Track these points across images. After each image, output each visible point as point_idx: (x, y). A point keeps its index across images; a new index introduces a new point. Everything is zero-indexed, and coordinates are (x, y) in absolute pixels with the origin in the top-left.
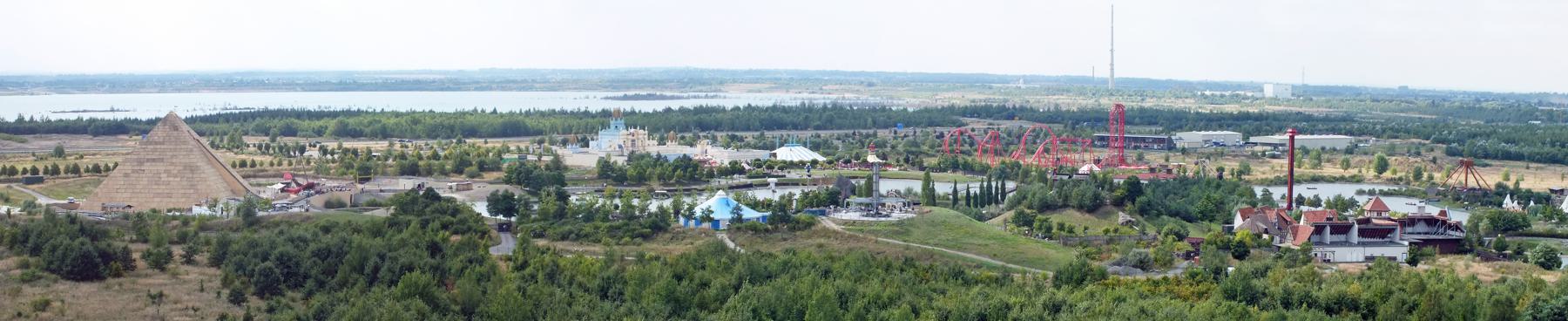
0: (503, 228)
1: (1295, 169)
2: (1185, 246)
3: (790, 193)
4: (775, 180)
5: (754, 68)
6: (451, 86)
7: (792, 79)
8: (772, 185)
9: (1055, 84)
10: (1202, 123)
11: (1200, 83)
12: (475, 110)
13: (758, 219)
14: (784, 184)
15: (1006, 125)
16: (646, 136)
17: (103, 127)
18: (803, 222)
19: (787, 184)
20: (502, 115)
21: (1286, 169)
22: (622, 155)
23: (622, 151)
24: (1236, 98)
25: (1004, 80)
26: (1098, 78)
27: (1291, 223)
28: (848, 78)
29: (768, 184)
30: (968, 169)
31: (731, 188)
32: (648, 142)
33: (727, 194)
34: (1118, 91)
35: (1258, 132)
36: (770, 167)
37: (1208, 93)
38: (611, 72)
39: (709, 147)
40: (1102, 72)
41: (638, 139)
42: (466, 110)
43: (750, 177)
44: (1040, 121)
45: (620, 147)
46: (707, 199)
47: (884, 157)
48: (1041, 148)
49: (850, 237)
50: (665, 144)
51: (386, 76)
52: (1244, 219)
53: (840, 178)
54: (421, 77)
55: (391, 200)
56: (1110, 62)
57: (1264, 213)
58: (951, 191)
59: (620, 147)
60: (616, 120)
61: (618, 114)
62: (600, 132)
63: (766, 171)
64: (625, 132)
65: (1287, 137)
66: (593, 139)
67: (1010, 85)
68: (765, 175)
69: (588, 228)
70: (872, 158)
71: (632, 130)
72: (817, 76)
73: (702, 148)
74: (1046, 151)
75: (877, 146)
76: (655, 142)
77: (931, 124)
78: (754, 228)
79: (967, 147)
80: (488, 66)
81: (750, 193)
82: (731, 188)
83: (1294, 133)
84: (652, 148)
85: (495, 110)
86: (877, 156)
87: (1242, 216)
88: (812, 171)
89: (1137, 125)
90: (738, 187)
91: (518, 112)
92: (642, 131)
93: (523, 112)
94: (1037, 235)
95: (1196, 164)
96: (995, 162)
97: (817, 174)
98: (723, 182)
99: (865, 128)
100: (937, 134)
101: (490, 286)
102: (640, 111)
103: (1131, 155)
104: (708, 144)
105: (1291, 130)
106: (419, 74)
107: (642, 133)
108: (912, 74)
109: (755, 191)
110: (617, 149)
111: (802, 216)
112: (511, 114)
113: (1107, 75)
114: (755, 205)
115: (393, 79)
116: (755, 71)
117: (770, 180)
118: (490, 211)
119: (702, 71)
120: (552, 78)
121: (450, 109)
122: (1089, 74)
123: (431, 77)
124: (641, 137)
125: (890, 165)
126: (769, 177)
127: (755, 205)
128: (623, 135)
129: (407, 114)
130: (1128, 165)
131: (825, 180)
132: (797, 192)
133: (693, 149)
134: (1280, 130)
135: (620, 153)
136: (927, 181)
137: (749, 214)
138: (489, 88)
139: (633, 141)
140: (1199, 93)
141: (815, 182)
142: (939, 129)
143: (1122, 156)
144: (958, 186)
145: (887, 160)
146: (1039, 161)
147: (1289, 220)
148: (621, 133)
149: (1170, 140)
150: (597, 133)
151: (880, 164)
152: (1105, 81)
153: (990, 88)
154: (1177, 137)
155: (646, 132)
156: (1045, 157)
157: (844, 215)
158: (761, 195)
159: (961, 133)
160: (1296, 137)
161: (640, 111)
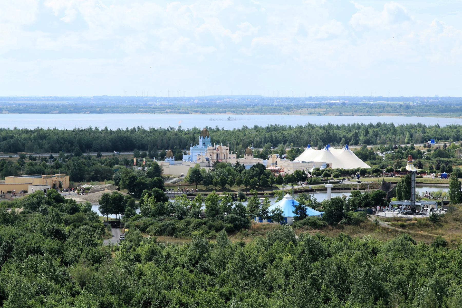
0: (116, 224)
3: (344, 195)
4: (331, 185)
5: (313, 96)
6: (72, 110)
7: (344, 104)
8: (329, 190)
9: (228, 100)
12: (134, 129)
13: (319, 216)
14: (339, 189)
16: (228, 151)
17: (58, 141)
18: (355, 219)
19: (342, 189)
20: (111, 132)
22: (209, 166)
23: (209, 163)
29: (326, 189)
31: (296, 192)
32: (229, 156)
33: (293, 197)
36: (327, 175)
38: (200, 99)
39: (279, 159)
41: (222, 153)
42: (83, 129)
43: (310, 184)
45: (207, 159)
46: (277, 201)
47: (420, 166)
49: (393, 231)
50: (243, 157)
51: (18, 102)
53: (384, 183)
54: (47, 102)
55: (22, 202)
59: (207, 159)
60: (204, 138)
61: (205, 133)
62: (191, 148)
64: (211, 147)
66: (185, 154)
68: (323, 182)
69: (180, 225)
70: (409, 168)
71: (217, 146)
72: (364, 101)
73: (273, 161)
75: (414, 157)
76: (235, 156)
78: (314, 225)
80: (100, 93)
82: (296, 192)
84: (232, 160)
85: (106, 128)
86: (415, 165)
88: (361, 178)
90: (301, 191)
91: (125, 129)
92: (224, 147)
93: (129, 129)
97: (365, 180)
98: (290, 187)
99: (403, 143)
102: (127, 129)
104: (277, 157)
106: (48, 100)
107: (224, 149)
109: (315, 195)
110: (205, 161)
111: (355, 215)
112: (119, 131)
114: (315, 206)
115: (24, 104)
116: (314, 98)
118: (102, 212)
119: (272, 99)
120: (152, 105)
121: (70, 128)
123: (56, 103)
124: (223, 151)
125: (424, 173)
126: (327, 183)
127: (315, 206)
128: (209, 150)
129: (35, 131)
131: (372, 186)
132: (348, 195)
133: (258, 161)
135: (207, 165)
137: (311, 212)
138: (101, 112)
139: (218, 155)
141: (364, 187)
148: (208, 148)
150: (189, 149)
155: (228, 148)
157: (390, 214)
158: (320, 198)
161: (127, 129)
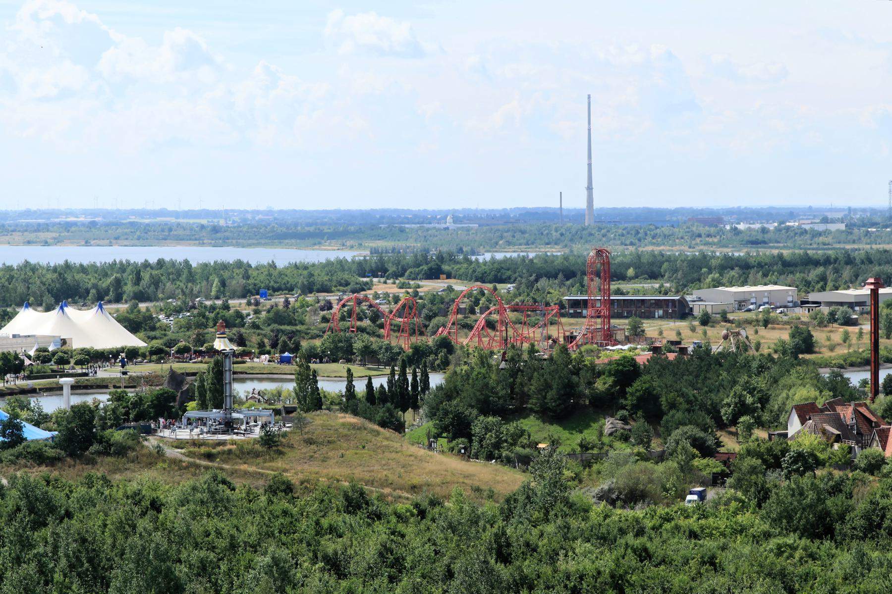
1: (880, 340)
2: (713, 465)
4: (70, 380)
7: (93, 224)
8: (66, 390)
10: (732, 273)
11: (730, 212)
13: (47, 440)
14: (86, 387)
15: (429, 286)
19: (92, 387)
21: (867, 340)
24: (786, 233)
25: (422, 219)
26: (568, 210)
27: (877, 425)
28: (181, 221)
29: (60, 388)
30: (369, 356)
34: (600, 229)
35: (823, 283)
36: (63, 361)
37: (742, 226)
40: (576, 202)
44: (482, 279)
47: (241, 341)
48: (481, 318)
52: (803, 421)
56: (585, 184)
57: (834, 410)
58: (344, 390)
63: (55, 367)
65: (866, 291)
67: (432, 225)
68: (54, 374)
70: (220, 344)
72: (133, 219)
74: (490, 325)
75: (228, 324)
77: (309, 289)
79: (366, 323)
81: (33, 401)
83: (878, 285)
87: (799, 416)
89: (631, 279)
90: (12, 392)
94: (840, 461)
95: (726, 337)
96: (404, 344)
97: (136, 370)
99: (208, 298)
100: (322, 303)
101: (810, 562)
103: (622, 324)
105: (872, 280)
108: (281, 212)
111: (118, 436)
113: (580, 204)
114: (40, 421)
116: (35, 212)
117: (63, 380)
122: (554, 204)
126: (61, 376)
130: (617, 342)
131: (150, 380)
132: (103, 399)
134: (855, 280)
136: (307, 379)
140: (728, 227)
142: (323, 296)
143: (609, 329)
144: (373, 381)
145: (245, 345)
146: (480, 341)
147: (873, 419)
149: (683, 303)
151: (234, 354)
152: (578, 216)
153: (402, 231)
154: (694, 297)
156: (488, 335)
158: (50, 405)
159: (359, 302)
160: (881, 291)
